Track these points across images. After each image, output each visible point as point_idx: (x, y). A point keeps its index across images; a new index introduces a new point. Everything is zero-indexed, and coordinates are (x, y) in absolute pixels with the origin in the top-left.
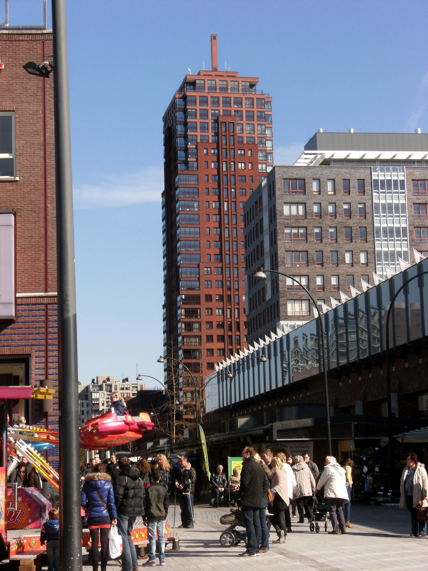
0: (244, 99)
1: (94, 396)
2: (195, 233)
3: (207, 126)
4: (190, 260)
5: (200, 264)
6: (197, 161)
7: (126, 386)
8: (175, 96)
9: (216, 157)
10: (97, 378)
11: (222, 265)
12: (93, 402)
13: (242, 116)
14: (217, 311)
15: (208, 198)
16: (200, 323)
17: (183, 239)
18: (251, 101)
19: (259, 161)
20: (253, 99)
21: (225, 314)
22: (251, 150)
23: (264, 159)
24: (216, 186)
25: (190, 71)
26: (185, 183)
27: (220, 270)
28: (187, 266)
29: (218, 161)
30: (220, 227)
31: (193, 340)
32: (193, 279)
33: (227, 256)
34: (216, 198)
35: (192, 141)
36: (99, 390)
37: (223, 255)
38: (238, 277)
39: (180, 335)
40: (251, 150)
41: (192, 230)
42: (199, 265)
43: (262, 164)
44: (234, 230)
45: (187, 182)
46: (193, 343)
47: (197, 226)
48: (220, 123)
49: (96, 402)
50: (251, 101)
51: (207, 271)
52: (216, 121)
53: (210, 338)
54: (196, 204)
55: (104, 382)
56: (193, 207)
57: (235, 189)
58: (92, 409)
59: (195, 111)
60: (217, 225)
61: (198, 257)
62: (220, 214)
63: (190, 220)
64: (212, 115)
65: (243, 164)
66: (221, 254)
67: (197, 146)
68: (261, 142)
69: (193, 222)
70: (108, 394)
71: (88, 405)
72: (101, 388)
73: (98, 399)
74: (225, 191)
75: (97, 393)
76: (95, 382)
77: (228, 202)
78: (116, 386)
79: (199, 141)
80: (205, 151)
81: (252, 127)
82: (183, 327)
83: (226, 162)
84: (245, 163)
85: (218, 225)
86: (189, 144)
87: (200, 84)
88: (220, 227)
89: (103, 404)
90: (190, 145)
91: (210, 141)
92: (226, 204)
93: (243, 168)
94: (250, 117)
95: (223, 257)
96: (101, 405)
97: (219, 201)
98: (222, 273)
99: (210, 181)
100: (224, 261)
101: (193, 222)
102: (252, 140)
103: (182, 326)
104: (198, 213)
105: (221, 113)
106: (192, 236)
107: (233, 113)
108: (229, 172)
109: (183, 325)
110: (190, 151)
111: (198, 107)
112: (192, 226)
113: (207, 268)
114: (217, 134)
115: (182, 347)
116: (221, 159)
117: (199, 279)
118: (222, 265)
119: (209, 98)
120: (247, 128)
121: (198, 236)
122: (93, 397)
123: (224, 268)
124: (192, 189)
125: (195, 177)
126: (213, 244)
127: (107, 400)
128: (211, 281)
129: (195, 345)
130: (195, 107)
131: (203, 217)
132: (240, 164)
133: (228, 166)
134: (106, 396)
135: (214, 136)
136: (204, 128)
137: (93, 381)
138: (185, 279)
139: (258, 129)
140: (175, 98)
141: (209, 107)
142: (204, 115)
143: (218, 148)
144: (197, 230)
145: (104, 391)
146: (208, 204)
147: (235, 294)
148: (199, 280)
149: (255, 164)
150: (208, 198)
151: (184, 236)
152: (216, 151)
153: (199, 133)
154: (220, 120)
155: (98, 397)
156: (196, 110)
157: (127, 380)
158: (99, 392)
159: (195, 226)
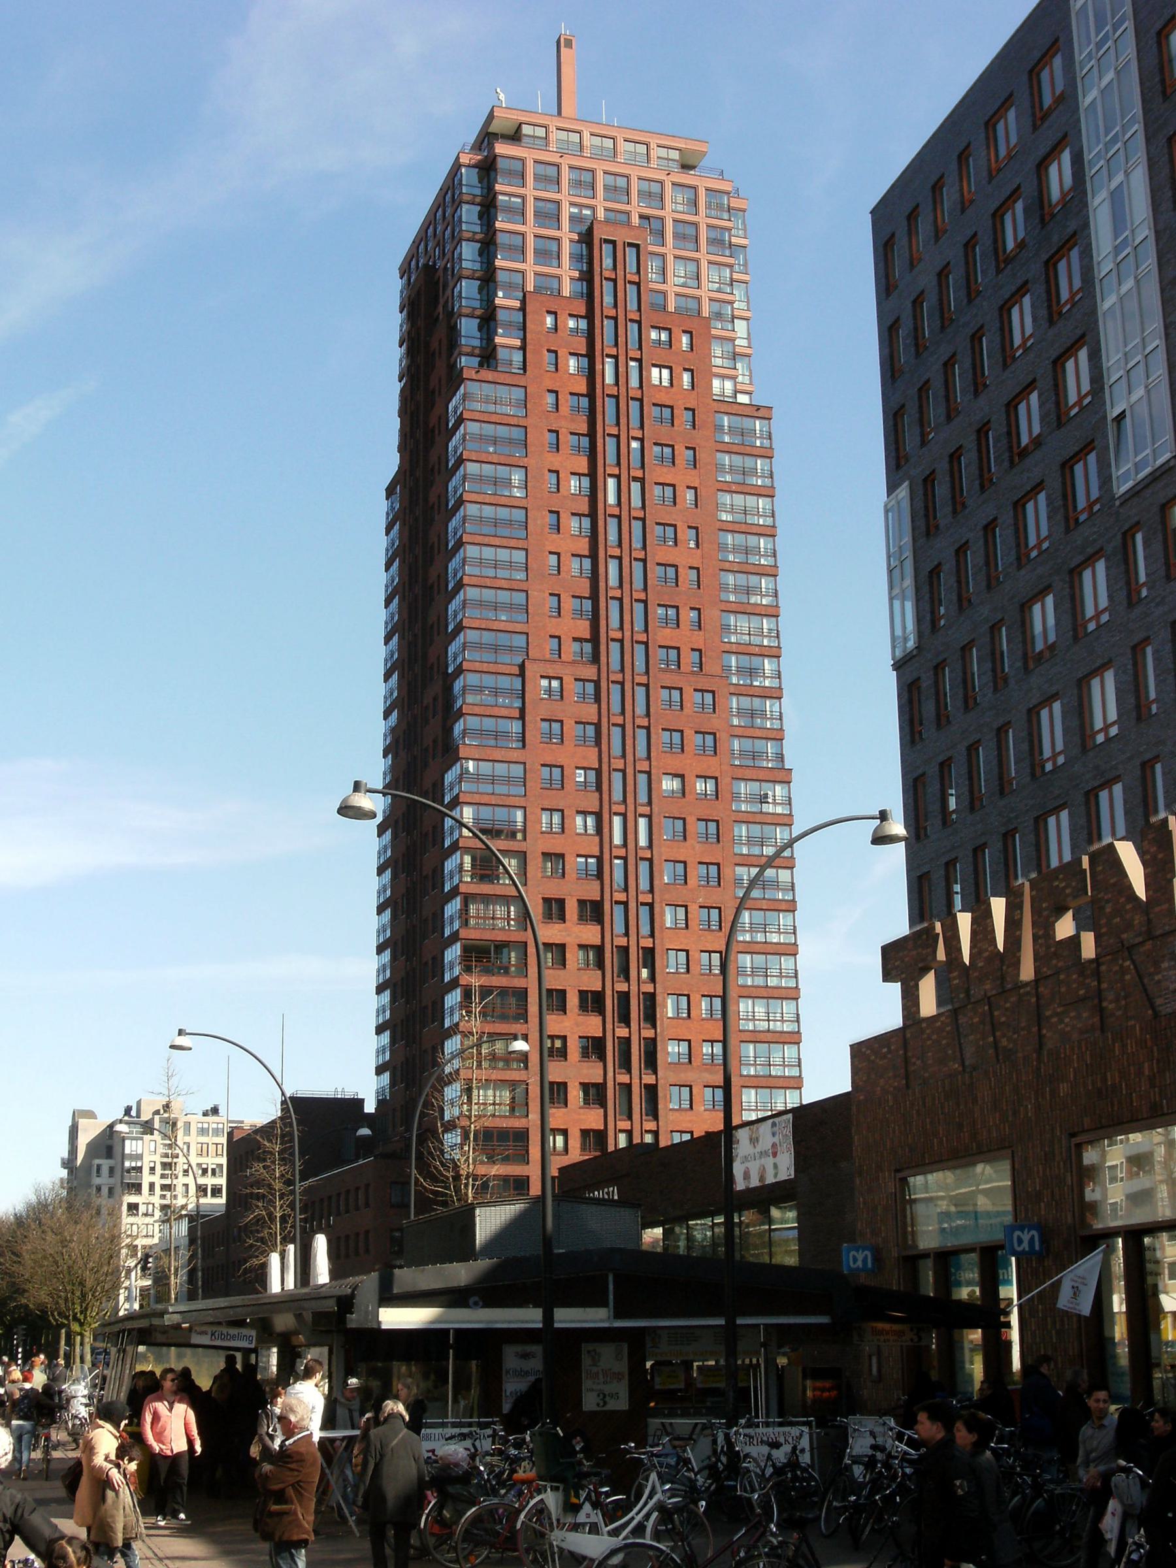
0: (668, 187)
1: (130, 1147)
2: (511, 565)
3: (555, 248)
4: (496, 649)
5: (530, 668)
6: (523, 348)
7: (215, 1126)
8: (458, 158)
9: (584, 340)
10: (139, 1103)
11: (599, 670)
12: (127, 1164)
13: (662, 233)
14: (579, 820)
15: (555, 461)
16: (522, 856)
17: (474, 581)
18: (690, 194)
19: (715, 370)
20: (695, 188)
21: (606, 830)
22: (691, 333)
23: (727, 363)
24: (583, 428)
25: (502, 96)
26: (484, 407)
27: (590, 687)
28: (485, 667)
29: (590, 355)
30: (593, 556)
31: (500, 911)
32: (504, 712)
33: (615, 647)
34: (582, 465)
35: (510, 287)
36: (144, 1133)
37: (603, 640)
38: (648, 715)
39: (455, 892)
40: (691, 333)
41: (503, 554)
42: (522, 667)
43: (723, 377)
44: (638, 567)
45: (491, 408)
46: (500, 922)
47: (520, 544)
48: (596, 242)
49: (133, 1164)
50: (690, 194)
51: (549, 690)
52: (587, 238)
53: (555, 908)
54: (517, 477)
55: (157, 1112)
56: (508, 483)
57: (642, 440)
58: (122, 1183)
59: (519, 200)
60: (583, 546)
61: (520, 641)
62: (593, 515)
63: (496, 523)
64: (573, 219)
65: (665, 372)
66: (595, 639)
67: (524, 302)
68: (719, 316)
69: (505, 532)
70: (165, 1145)
71: (112, 1170)
72: (148, 1128)
73: (140, 1157)
74: (611, 443)
75: (136, 1139)
76: (133, 1113)
77: (618, 477)
78: (188, 1125)
79: (530, 287)
80: (549, 321)
81: (692, 267)
82: (467, 865)
83: (616, 357)
84: (670, 368)
85: (587, 546)
86: (500, 294)
87: (534, 137)
88: (593, 556)
89: (152, 1169)
90: (500, 299)
91: (566, 292)
92: (611, 483)
93: (666, 383)
94: (688, 235)
95: (603, 648)
96: (146, 1171)
97: (592, 474)
98: (598, 699)
99: (564, 409)
100: (603, 659)
101: (505, 532)
102: (692, 304)
103: (462, 864)
104: (523, 503)
105: (601, 214)
106: (501, 573)
107: (635, 220)
108: (623, 390)
109: (467, 859)
110: (501, 315)
111: (530, 191)
112: (504, 542)
113: (550, 678)
114: (587, 277)
115: (463, 934)
116: (598, 346)
117: (522, 710)
118: (599, 670)
119: (565, 171)
120: (678, 274)
121: (521, 576)
122: (127, 1151)
123: (604, 684)
124: (507, 428)
125: (518, 393)
126: (569, 604)
127: (165, 1160)
128: (561, 722)
129: (503, 929)
130: (521, 191)
131: (541, 520)
132: (655, 372)
133: (622, 369)
134: (161, 1150)
135: (579, 279)
136: (545, 255)
137: (128, 1111)
138: (477, 710)
139: (712, 278)
140: (457, 166)
141: (565, 196)
142: (549, 215)
143: (590, 316)
144: (519, 556)
145: (157, 1136)
146: (554, 481)
147: (638, 768)
148: (522, 717)
149: (700, 374)
150: (555, 461)
151: (476, 571)
152: (583, 324)
153: (530, 266)
154: (598, 234)
155: (139, 1152)
156: (523, 198)
157: (215, 1111)
158: (142, 1139)
159: (512, 543)
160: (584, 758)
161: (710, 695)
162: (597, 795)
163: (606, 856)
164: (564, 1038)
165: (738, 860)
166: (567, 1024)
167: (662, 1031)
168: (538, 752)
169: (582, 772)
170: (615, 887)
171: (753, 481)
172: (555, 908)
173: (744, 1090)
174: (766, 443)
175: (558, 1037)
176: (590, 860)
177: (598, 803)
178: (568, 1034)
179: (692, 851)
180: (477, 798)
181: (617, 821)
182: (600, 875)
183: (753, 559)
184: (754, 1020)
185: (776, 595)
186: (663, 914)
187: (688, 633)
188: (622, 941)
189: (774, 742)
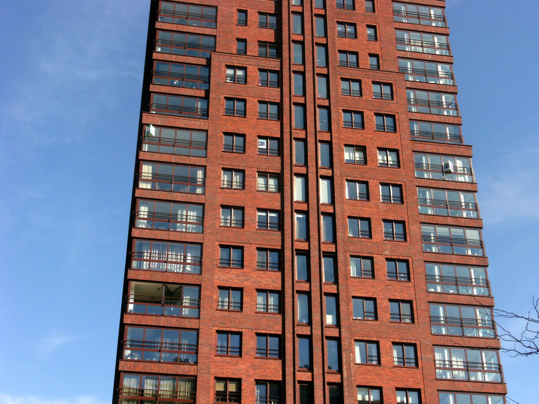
5: (216, 59)
15: (231, 277)
21: (287, 188)
98: (282, 355)
147: (319, 138)
160: (266, 129)
161: (412, 349)
162: (279, 159)
163: (287, 210)
164: (238, 381)
165: (423, 219)
166: (243, 367)
167: (349, 376)
168: (220, 122)
169: (265, 141)
170: (298, 364)
171: (472, 333)
172: (234, 254)
173: (436, 348)
174: (473, 215)
175: (232, 380)
176: (270, 215)
177: (279, 166)
178: (243, 377)
179: (383, 289)
180: (157, 157)
181: (298, 183)
182: (281, 226)
183: (469, 333)
184: (451, 369)
185: (487, 285)
186: (347, 265)
187: (366, 43)
188: (306, 376)
189: (452, 127)
